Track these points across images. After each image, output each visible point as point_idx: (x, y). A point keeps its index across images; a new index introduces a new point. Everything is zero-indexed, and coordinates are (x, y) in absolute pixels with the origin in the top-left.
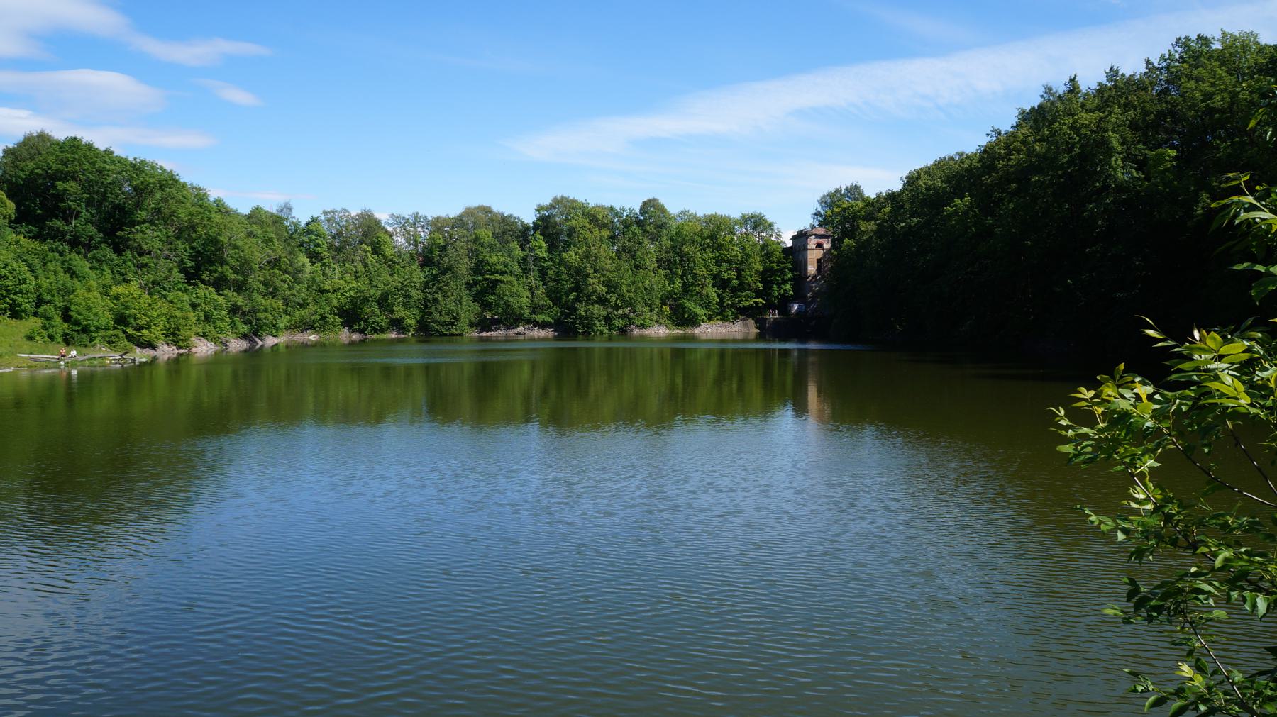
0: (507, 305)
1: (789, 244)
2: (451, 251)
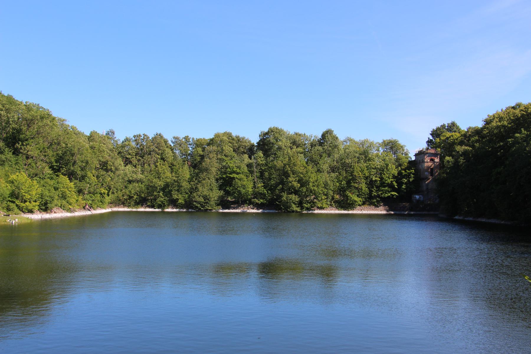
0: (239, 192)
1: (413, 158)
2: (207, 160)
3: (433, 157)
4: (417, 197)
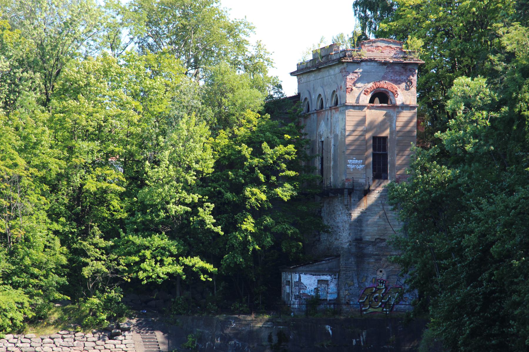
1: (291, 88)
3: (385, 84)
4: (309, 282)
